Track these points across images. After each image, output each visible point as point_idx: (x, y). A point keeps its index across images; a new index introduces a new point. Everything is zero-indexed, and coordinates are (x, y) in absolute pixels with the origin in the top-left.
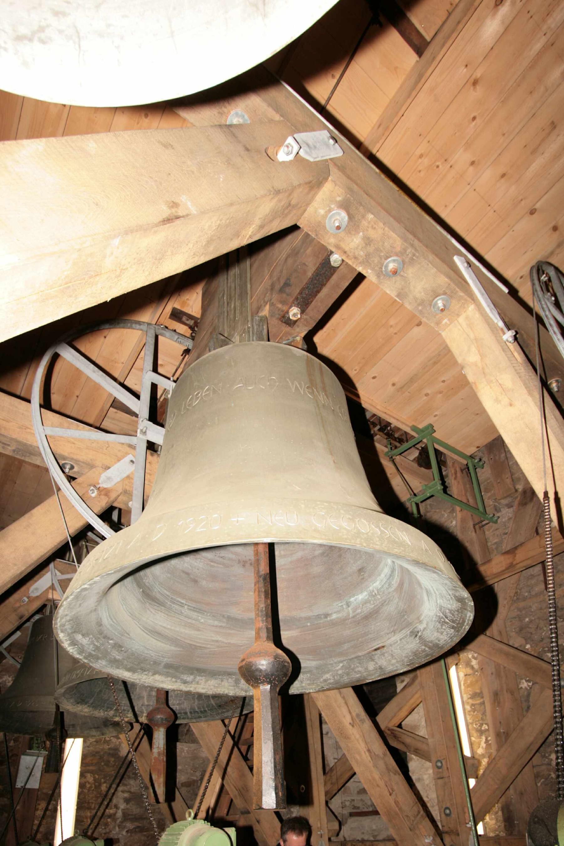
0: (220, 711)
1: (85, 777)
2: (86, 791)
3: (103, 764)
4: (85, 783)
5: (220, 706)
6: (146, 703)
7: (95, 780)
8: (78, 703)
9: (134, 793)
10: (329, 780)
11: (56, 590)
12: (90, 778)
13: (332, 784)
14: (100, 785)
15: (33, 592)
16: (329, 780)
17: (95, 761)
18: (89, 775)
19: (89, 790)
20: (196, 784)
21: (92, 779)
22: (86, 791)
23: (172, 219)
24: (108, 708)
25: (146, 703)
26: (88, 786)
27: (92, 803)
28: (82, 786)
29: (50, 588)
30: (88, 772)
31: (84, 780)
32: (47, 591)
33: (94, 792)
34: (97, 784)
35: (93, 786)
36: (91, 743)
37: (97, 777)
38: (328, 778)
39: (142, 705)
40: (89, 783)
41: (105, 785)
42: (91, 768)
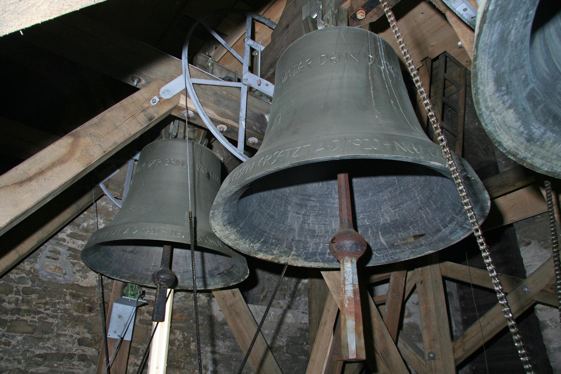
0: (390, 252)
1: (175, 334)
2: (175, 348)
3: (191, 321)
4: (175, 340)
5: (393, 245)
6: (297, 238)
7: (184, 338)
8: (229, 223)
9: (222, 355)
10: (460, 347)
11: (190, 97)
12: (179, 335)
13: (464, 351)
14: (189, 343)
15: (164, 92)
16: (460, 347)
17: (183, 318)
18: (178, 332)
19: (178, 348)
20: (282, 350)
21: (181, 336)
22: (175, 348)
23: (8, 186)
24: (255, 238)
25: (297, 238)
26: (177, 343)
27: (182, 362)
28: (171, 343)
29: (181, 92)
30: (177, 328)
31: (173, 337)
32: (178, 95)
33: (184, 351)
34: (186, 342)
35: (182, 344)
36: (180, 299)
37: (186, 335)
38: (459, 343)
39: (292, 240)
40: (178, 340)
41: (194, 344)
42: (180, 325)
